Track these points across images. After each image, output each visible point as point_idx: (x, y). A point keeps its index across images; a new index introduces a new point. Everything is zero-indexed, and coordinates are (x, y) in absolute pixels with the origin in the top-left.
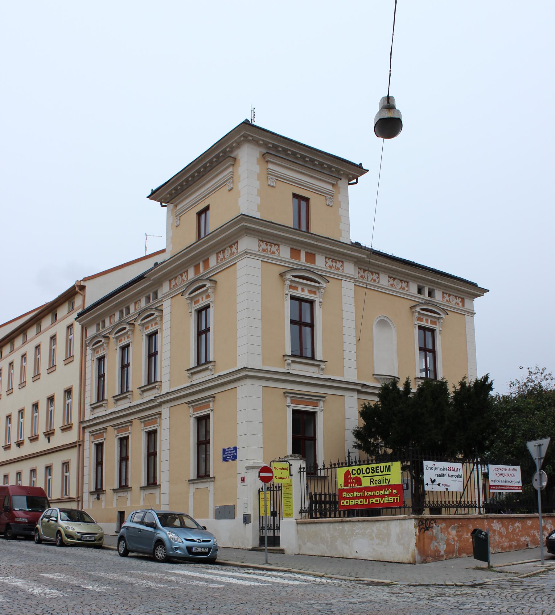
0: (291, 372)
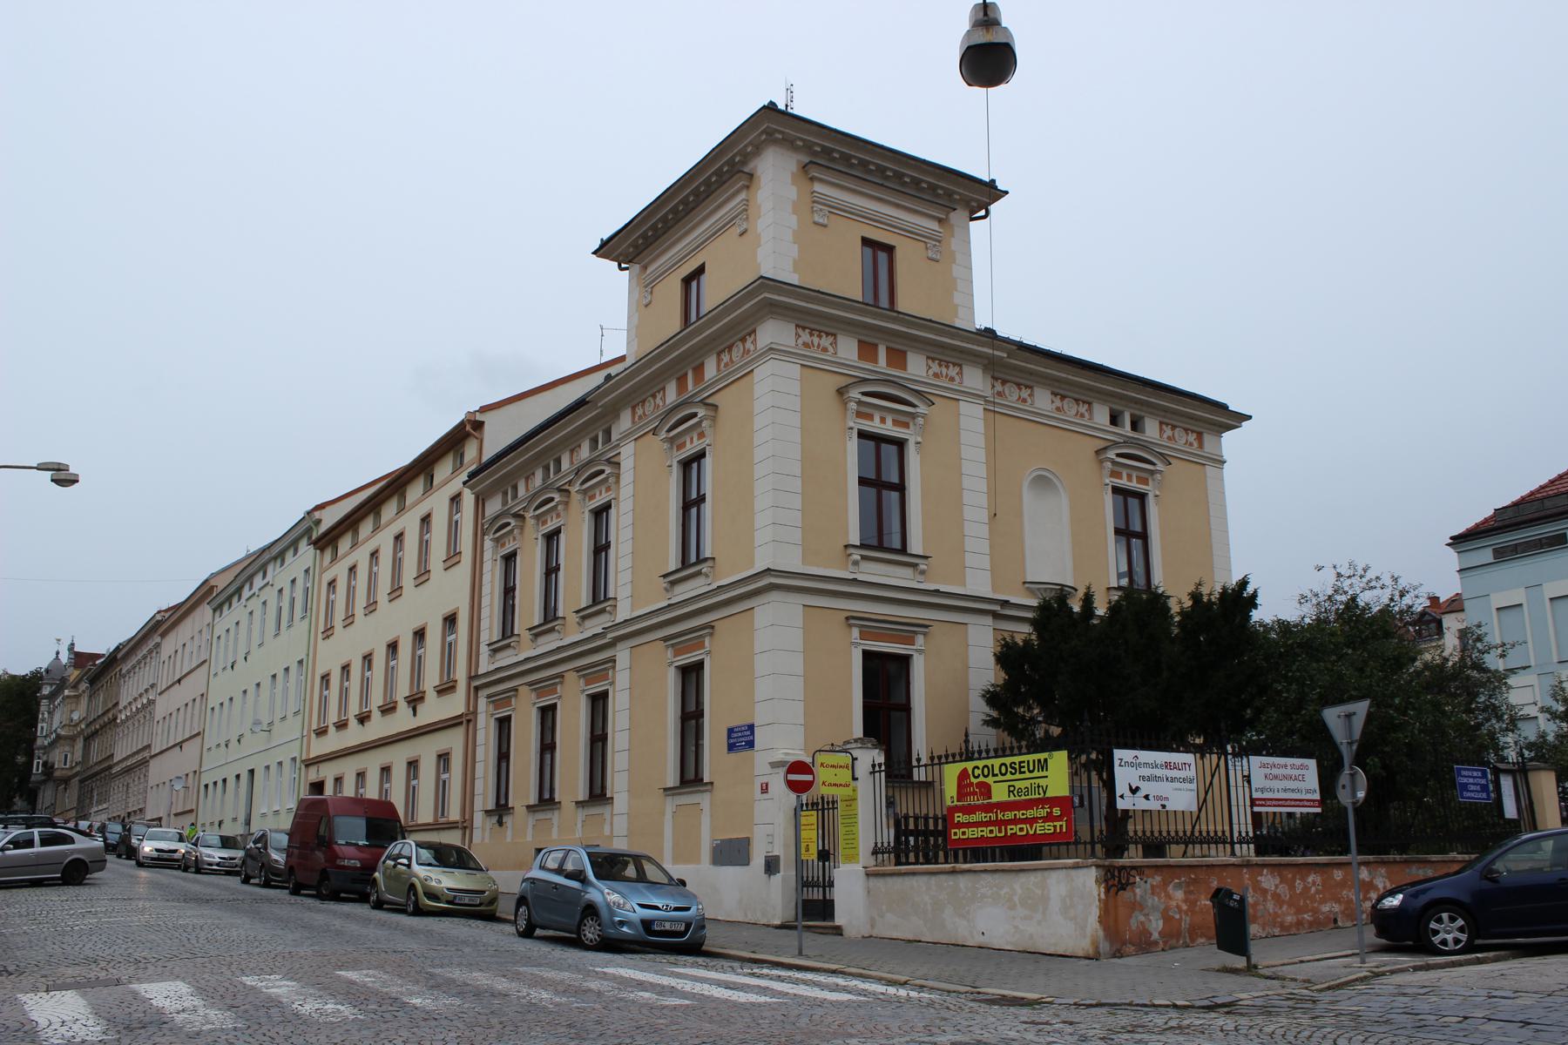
0: (860, 577)
